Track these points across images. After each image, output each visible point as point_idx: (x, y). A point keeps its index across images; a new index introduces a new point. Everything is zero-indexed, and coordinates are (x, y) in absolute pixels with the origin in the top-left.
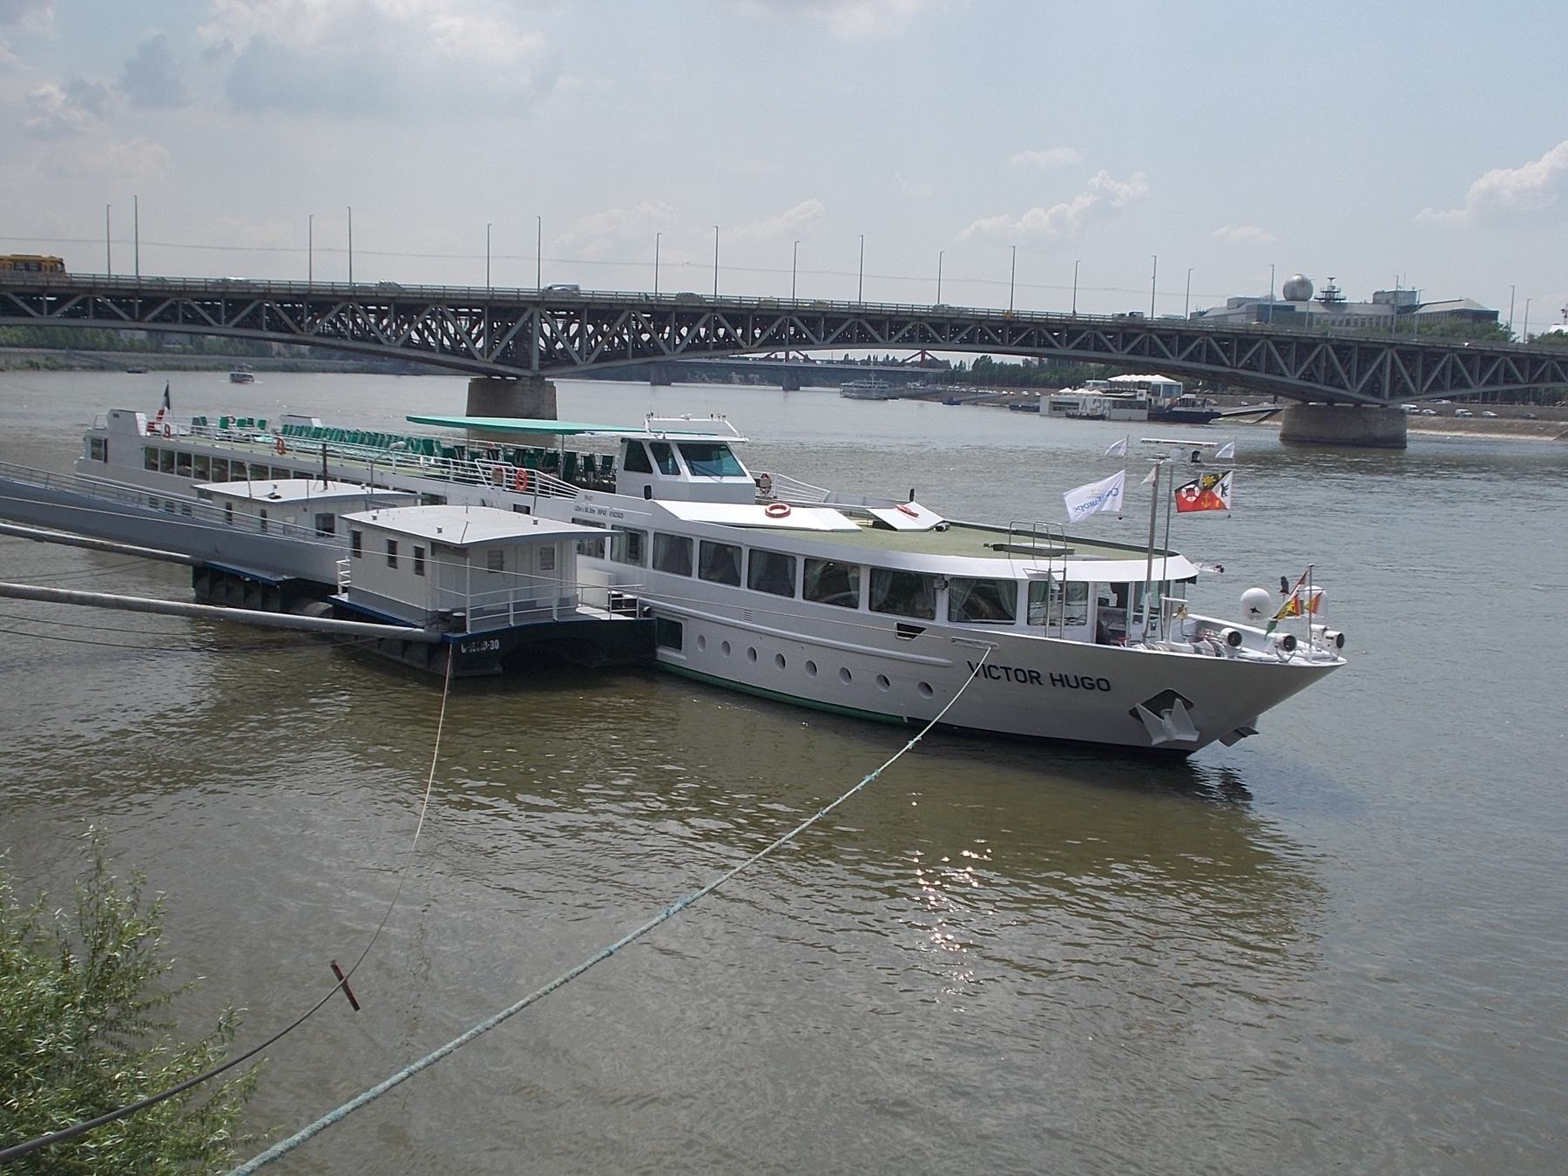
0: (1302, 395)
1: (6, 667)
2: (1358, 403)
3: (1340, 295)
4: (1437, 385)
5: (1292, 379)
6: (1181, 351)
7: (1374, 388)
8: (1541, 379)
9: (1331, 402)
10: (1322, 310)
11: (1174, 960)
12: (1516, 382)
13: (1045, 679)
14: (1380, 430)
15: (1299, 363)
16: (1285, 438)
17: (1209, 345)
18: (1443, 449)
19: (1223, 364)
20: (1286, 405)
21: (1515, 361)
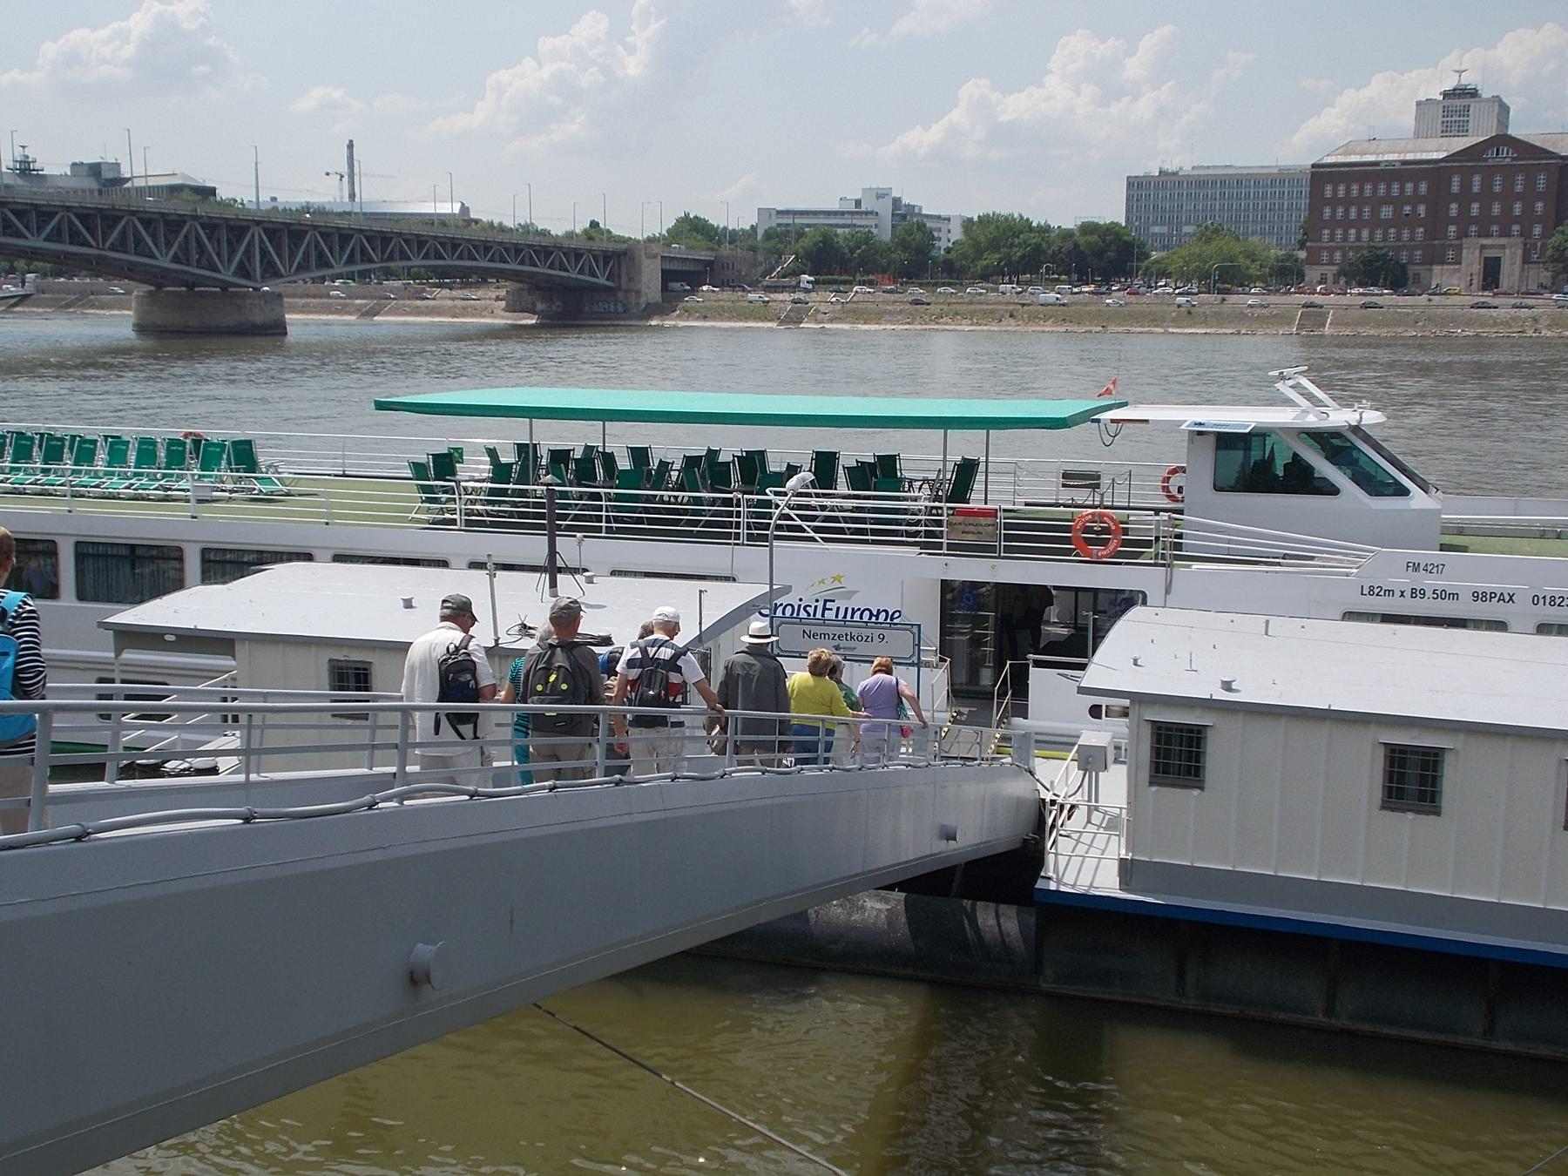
0: (157, 278)
1: (25, 562)
2: (225, 286)
3: (37, 166)
4: (303, 267)
5: (165, 262)
6: (40, 229)
7: (244, 271)
8: (391, 258)
9: (191, 286)
10: (20, 182)
11: (110, 769)
12: (371, 261)
13: (1429, 593)
14: (258, 317)
15: (169, 244)
16: (141, 328)
17: (71, 223)
18: (402, 332)
19: (89, 246)
20: (140, 290)
21: (367, 238)
